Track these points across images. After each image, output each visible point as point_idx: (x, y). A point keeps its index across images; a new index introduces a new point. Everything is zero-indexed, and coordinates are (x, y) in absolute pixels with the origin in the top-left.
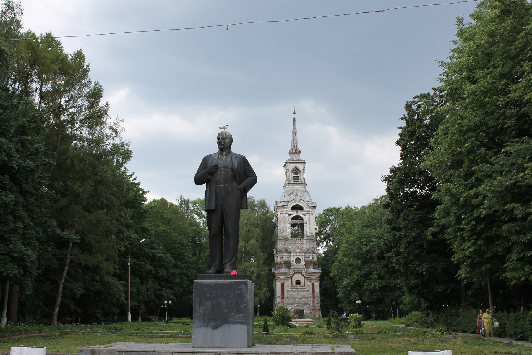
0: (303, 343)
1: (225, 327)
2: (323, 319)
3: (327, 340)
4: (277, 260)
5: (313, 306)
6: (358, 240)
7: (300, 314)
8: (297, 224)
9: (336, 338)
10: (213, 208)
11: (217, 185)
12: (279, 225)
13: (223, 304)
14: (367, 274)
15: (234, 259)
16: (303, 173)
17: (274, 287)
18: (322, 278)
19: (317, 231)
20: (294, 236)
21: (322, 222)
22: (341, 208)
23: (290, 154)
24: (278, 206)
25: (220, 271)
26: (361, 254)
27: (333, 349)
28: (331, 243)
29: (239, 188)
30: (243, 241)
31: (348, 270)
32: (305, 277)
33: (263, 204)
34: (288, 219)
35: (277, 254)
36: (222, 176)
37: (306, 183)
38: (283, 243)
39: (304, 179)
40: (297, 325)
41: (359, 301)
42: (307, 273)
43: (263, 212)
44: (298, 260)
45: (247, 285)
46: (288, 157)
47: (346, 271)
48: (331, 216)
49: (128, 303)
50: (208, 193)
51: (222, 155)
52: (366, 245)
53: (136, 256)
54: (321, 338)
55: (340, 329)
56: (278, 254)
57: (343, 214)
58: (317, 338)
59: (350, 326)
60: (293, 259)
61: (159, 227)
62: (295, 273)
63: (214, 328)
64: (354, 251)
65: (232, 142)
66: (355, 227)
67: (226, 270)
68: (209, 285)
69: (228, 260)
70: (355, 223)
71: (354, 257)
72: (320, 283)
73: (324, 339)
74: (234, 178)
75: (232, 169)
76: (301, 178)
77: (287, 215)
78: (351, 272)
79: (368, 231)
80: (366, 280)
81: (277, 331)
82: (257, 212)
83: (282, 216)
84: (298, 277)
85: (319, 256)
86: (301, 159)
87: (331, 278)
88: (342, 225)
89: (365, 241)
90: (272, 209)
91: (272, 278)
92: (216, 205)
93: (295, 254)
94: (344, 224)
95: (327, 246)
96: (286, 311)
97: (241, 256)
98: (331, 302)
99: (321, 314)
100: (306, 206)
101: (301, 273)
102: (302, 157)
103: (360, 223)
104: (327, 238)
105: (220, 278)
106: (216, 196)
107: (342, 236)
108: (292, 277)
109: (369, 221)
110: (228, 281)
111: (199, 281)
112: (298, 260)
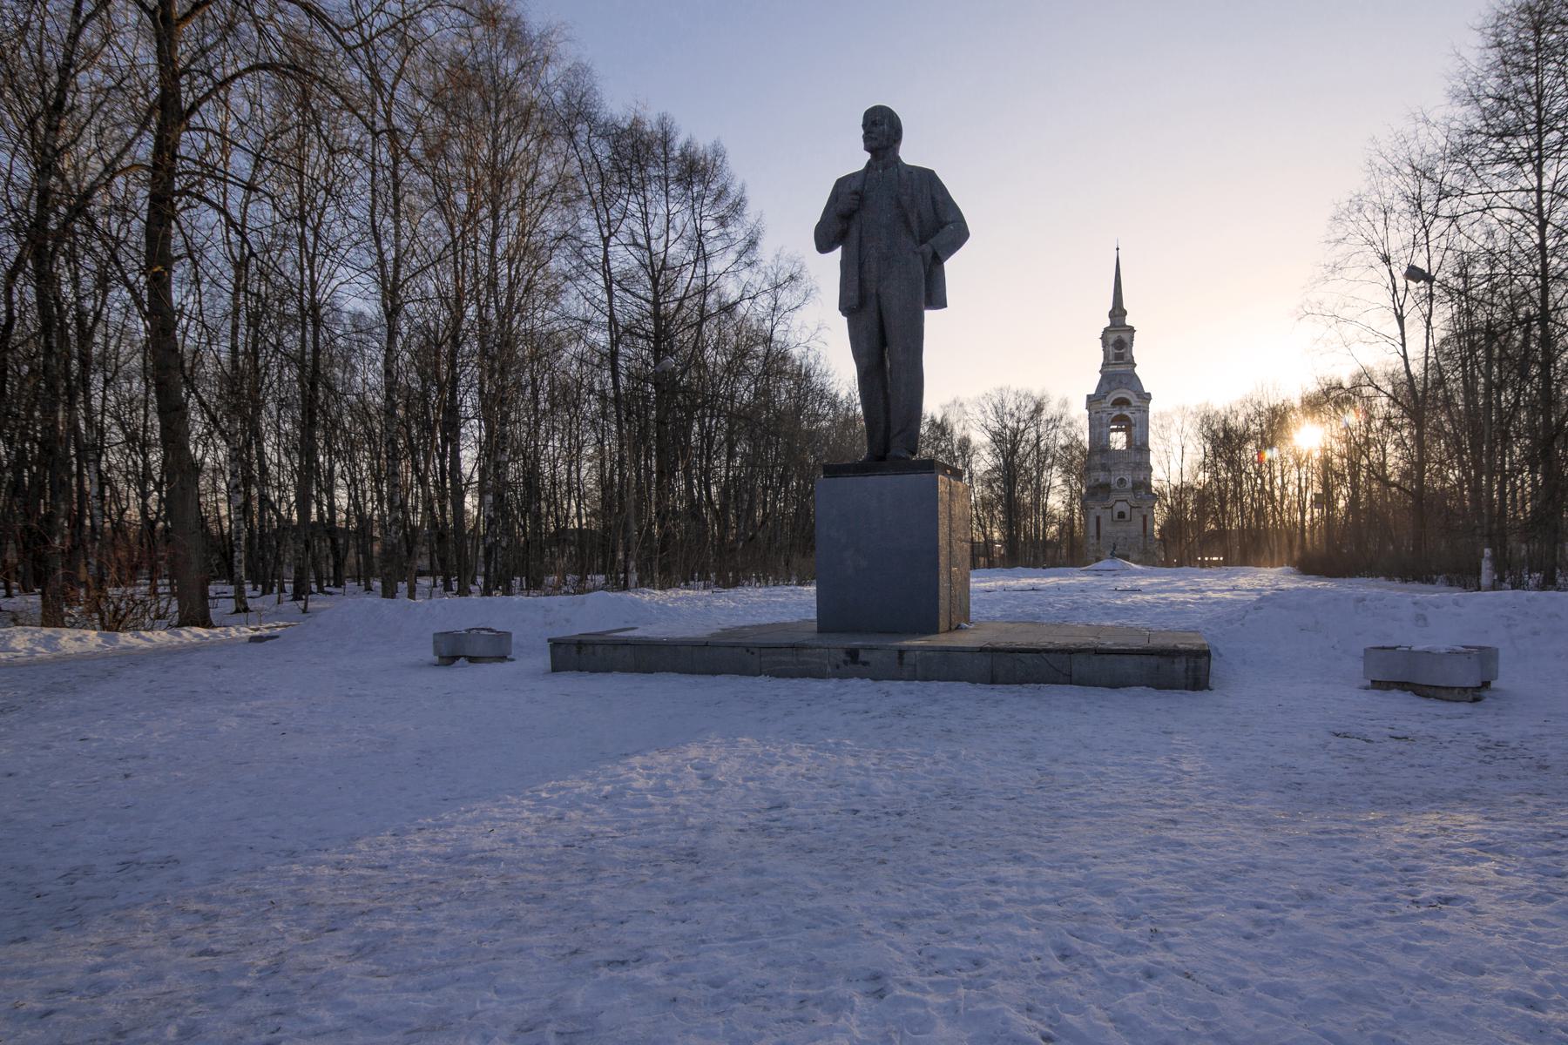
84: (1120, 507)
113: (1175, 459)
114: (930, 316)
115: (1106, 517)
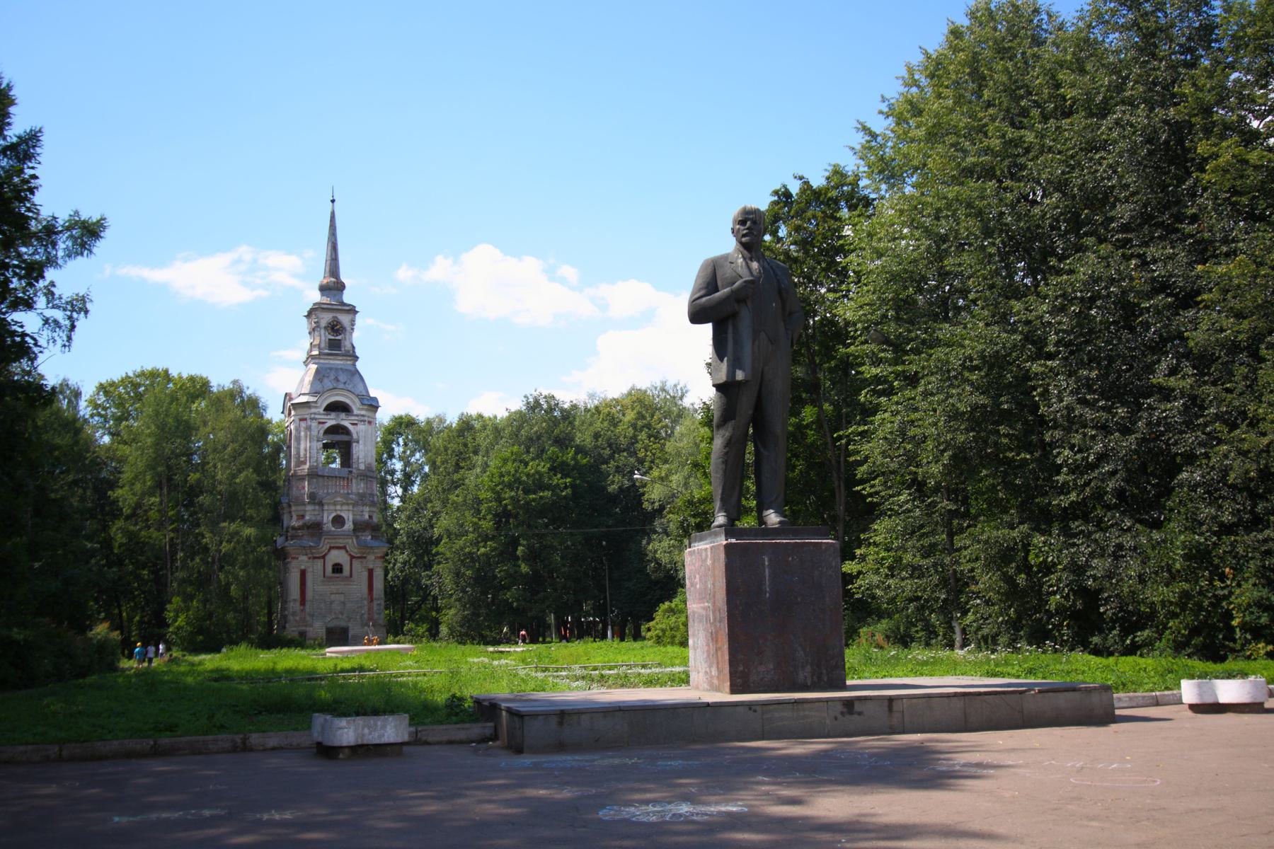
32: (352, 557)
84: (337, 556)
101: (344, 548)
102: (347, 297)
108: (324, 557)
115: (315, 570)
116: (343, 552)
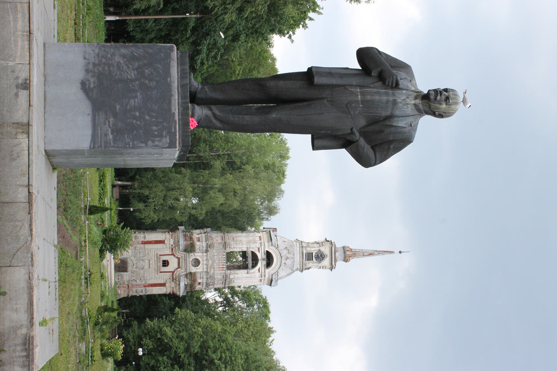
0: (60, 264)
1: (85, 106)
2: (115, 300)
3: (76, 308)
4: (196, 234)
5: (133, 286)
6: (227, 346)
7: (121, 267)
8: (246, 260)
9: (79, 322)
10: (317, 80)
11: (361, 87)
12: (244, 234)
13: (132, 102)
14: (179, 361)
15: (218, 124)
16: (317, 266)
17: (157, 230)
18: (172, 296)
19: (237, 289)
20: (230, 256)
21: (248, 295)
22: (269, 321)
23: (344, 248)
24: (270, 233)
25: (194, 99)
26: (207, 351)
27: (43, 323)
28: (221, 309)
29: (355, 130)
30: (222, 185)
31: (184, 334)
32: (173, 272)
33: (272, 211)
34: (254, 248)
35: (205, 233)
36: (377, 98)
37: (304, 271)
38: (220, 241)
39: (309, 269)
40: (105, 262)
41: (141, 353)
42: (179, 277)
43: (262, 212)
44: (197, 263)
45: (169, 147)
46: (339, 245)
47: (183, 330)
48: (259, 308)
49: (130, 15)
50: (344, 72)
51: (416, 98)
52: (220, 359)
53: (200, 23)
54: (80, 297)
55: (98, 328)
56: (204, 235)
57: (261, 324)
58: (80, 290)
59: (105, 341)
60: (198, 255)
61: (239, 65)
62: (179, 259)
63: (83, 85)
64: (212, 341)
65: (441, 116)
66: (246, 342)
67: (197, 108)
68: (167, 73)
69: (217, 113)
70: (251, 342)
71: (204, 342)
72: (165, 295)
73: (77, 303)
74: (374, 121)
75: (390, 117)
76: (310, 264)
77: (258, 245)
78: (182, 338)
79: (240, 361)
80: (171, 359)
81: (92, 229)
82: (262, 204)
83: (258, 239)
84: (173, 263)
85: (202, 292)
86: (337, 263)
87: (172, 310)
88: (246, 323)
89: (226, 357)
90: (266, 224)
91: (171, 226)
92: (322, 87)
93: (205, 258)
94: (249, 326)
95: (216, 302)
96: (125, 245)
97: (200, 183)
98: (139, 310)
99: (122, 296)
100: (272, 272)
101: (179, 267)
102: (340, 264)
103: (252, 349)
104: (227, 303)
105: (182, 96)
106: (339, 86)
107: (231, 323)
108: (173, 254)
109: (254, 362)
110: (175, 109)
111: (175, 54)
112: (197, 263)
113: (24, 354)
114: (308, 137)
116: (177, 267)
